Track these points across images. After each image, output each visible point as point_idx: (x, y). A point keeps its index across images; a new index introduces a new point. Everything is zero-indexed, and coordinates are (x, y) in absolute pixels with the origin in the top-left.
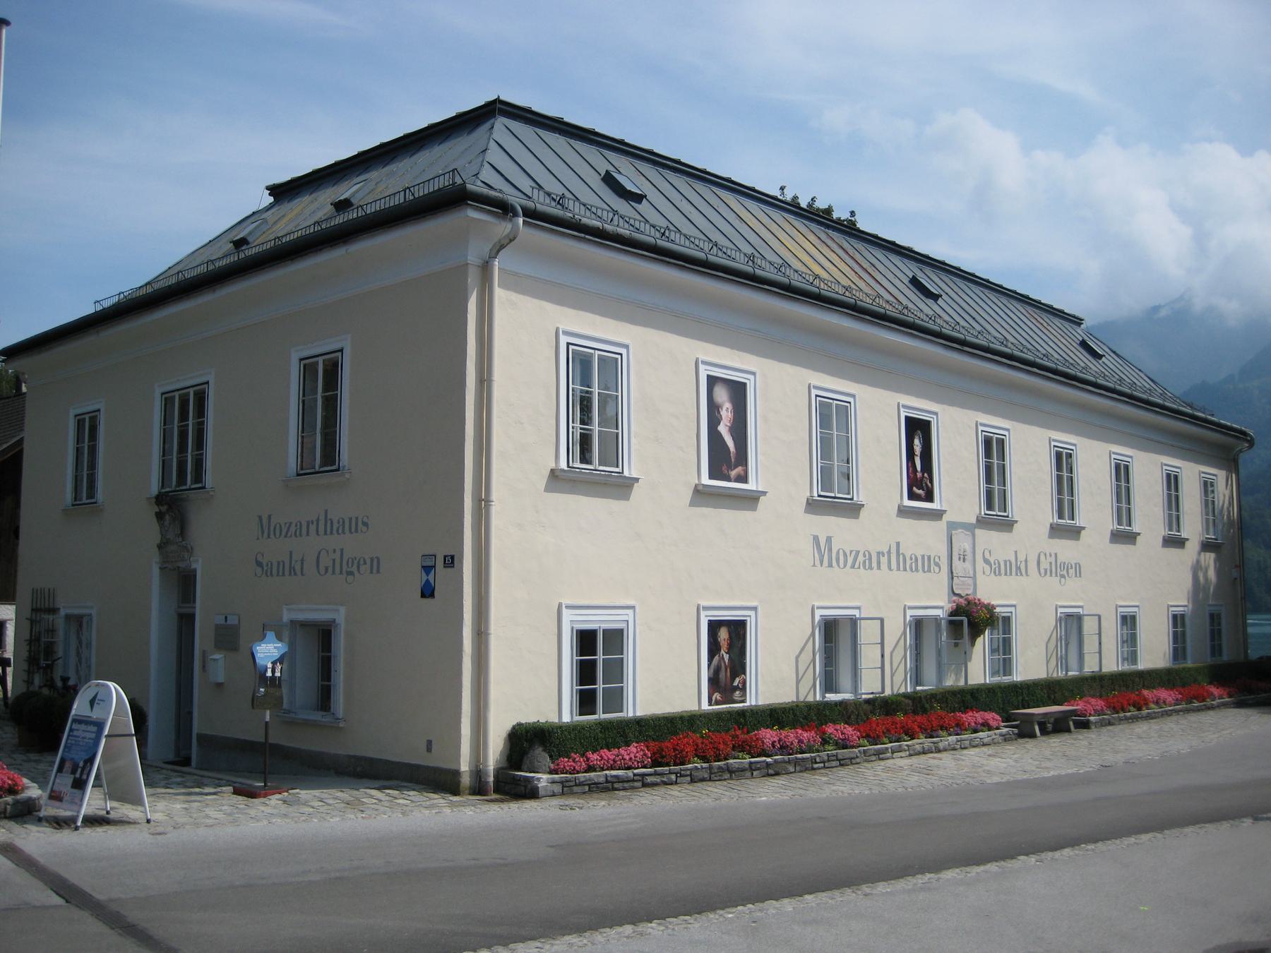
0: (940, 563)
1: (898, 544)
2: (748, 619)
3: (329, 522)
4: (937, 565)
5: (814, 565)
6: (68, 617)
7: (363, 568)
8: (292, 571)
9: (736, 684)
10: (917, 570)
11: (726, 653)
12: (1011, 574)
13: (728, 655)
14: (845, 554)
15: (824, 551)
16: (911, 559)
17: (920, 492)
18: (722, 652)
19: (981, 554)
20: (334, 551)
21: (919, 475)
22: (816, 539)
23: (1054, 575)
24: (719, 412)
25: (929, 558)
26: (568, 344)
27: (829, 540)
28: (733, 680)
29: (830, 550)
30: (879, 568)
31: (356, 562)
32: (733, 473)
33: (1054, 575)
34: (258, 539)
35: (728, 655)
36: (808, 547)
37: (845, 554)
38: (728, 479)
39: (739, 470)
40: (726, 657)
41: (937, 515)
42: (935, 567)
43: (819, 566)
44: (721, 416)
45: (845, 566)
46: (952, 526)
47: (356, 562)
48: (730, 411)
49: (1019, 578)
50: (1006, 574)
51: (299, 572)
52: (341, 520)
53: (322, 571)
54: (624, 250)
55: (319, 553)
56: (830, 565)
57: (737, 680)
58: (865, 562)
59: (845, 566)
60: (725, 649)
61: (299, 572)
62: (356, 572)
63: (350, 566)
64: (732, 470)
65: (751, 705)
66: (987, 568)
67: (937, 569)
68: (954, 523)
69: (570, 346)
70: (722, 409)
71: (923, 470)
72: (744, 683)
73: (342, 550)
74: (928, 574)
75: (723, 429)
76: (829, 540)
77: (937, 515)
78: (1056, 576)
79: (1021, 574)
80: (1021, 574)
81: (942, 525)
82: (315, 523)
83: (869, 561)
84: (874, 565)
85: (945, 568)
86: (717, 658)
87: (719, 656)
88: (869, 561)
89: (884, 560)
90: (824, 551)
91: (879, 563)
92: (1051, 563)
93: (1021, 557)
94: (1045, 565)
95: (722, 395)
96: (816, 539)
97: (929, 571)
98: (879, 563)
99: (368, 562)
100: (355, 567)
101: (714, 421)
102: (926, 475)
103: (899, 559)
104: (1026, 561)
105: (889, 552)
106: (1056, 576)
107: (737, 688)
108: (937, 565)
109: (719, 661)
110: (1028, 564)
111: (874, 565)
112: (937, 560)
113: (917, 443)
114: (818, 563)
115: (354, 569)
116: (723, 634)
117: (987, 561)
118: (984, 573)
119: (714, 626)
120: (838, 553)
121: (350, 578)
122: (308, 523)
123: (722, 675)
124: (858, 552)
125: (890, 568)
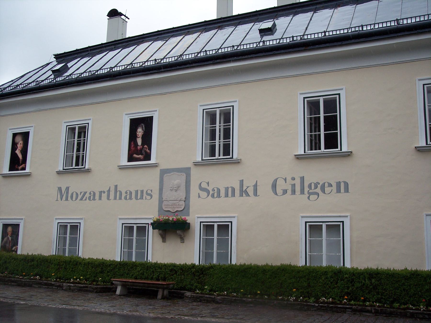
0: (152, 194)
2: (82, 222)
3: (118, 194)
5: (57, 200)
7: (327, 189)
8: (243, 192)
9: (13, 249)
11: (10, 237)
13: (11, 238)
14: (77, 194)
18: (9, 236)
22: (60, 189)
24: (17, 146)
26: (88, 123)
28: (12, 247)
29: (68, 193)
31: (319, 186)
32: (20, 167)
34: (57, 200)
35: (11, 238)
36: (55, 192)
38: (18, 170)
39: (23, 165)
40: (10, 238)
42: (147, 196)
43: (60, 200)
44: (17, 147)
45: (76, 199)
46: (163, 172)
48: (21, 144)
49: (245, 198)
52: (92, 193)
53: (279, 190)
54: (41, 91)
55: (276, 180)
56: (67, 199)
57: (14, 248)
58: (90, 197)
59: (76, 199)
60: (10, 235)
64: (20, 166)
65: (248, 265)
66: (204, 194)
69: (87, 124)
70: (18, 144)
71: (143, 144)
77: (155, 166)
78: (302, 192)
79: (248, 195)
80: (248, 195)
81: (156, 172)
82: (106, 193)
85: (156, 196)
87: (7, 238)
89: (104, 196)
95: (20, 141)
96: (60, 189)
99: (334, 185)
104: (255, 186)
105: (109, 191)
106: (302, 192)
107: (14, 251)
109: (7, 240)
115: (318, 190)
116: (10, 229)
119: (5, 226)
120: (72, 194)
121: (313, 197)
122: (101, 192)
124: (85, 193)
125: (108, 198)
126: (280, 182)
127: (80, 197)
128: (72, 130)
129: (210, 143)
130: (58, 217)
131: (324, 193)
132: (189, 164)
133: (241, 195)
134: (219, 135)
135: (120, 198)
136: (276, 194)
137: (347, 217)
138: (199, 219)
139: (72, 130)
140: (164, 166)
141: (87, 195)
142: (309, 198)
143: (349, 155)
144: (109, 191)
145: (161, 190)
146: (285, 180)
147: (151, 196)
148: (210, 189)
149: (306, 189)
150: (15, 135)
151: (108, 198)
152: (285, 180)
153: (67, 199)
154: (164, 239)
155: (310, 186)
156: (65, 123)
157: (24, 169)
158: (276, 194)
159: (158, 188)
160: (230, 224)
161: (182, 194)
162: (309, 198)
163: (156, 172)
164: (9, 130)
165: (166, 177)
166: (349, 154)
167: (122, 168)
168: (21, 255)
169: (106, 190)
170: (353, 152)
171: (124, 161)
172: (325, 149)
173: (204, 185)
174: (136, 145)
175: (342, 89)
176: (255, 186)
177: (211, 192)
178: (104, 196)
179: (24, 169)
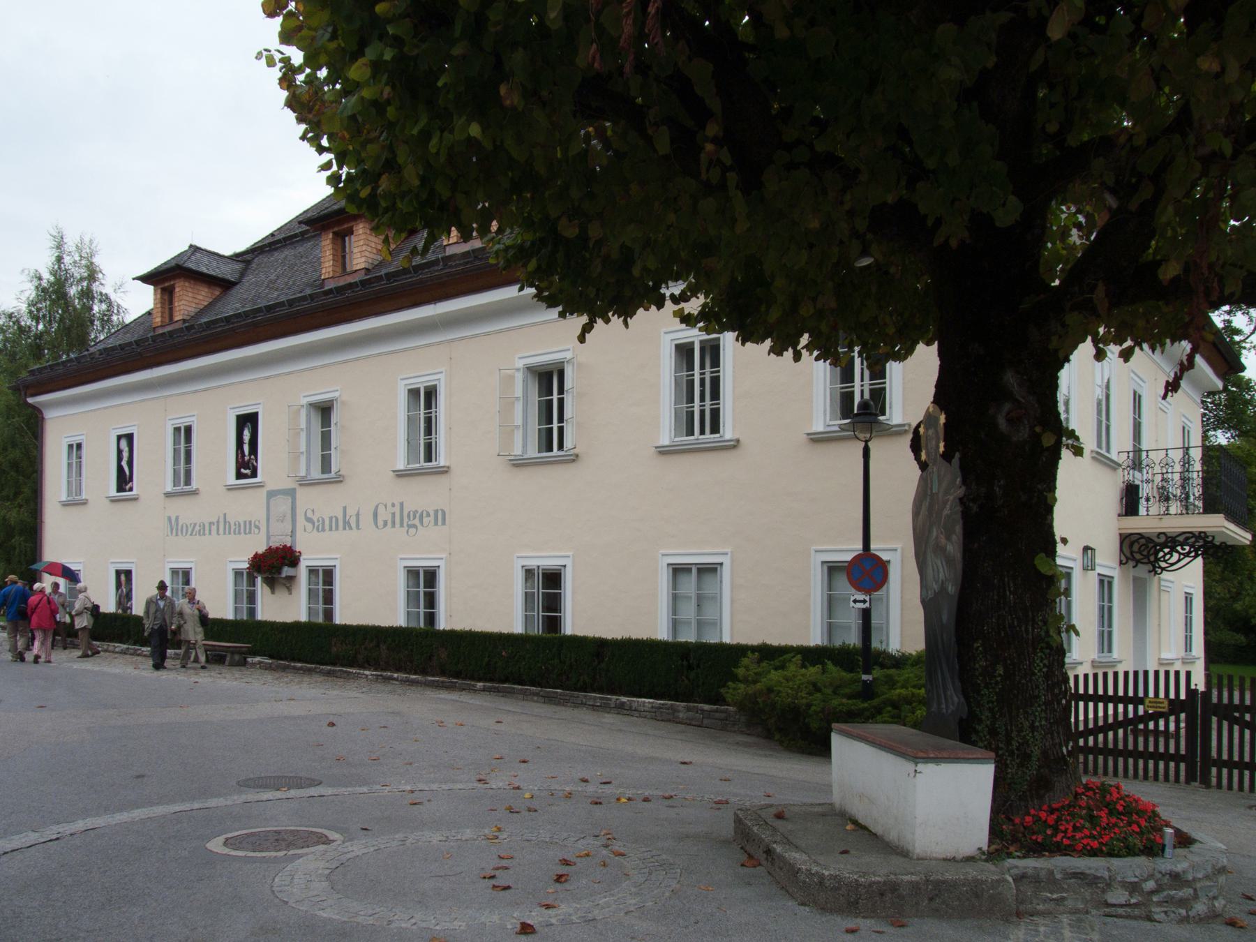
1: (225, 515)
4: (258, 528)
6: (313, 571)
7: (426, 520)
8: (347, 524)
10: (240, 533)
12: (337, 529)
14: (187, 526)
15: (174, 526)
16: (235, 525)
17: (247, 471)
19: (303, 514)
20: (393, 505)
21: (247, 458)
22: (169, 519)
23: (398, 525)
25: (250, 522)
27: (177, 518)
29: (177, 525)
30: (210, 534)
31: (418, 515)
33: (398, 525)
37: (187, 526)
40: (124, 590)
41: (260, 486)
45: (186, 534)
46: (271, 494)
47: (418, 515)
49: (348, 532)
50: (331, 529)
51: (354, 525)
53: (380, 523)
55: (377, 507)
56: (177, 535)
58: (200, 531)
59: (186, 534)
61: (354, 525)
62: (418, 525)
63: (412, 518)
66: (309, 526)
67: (257, 531)
68: (273, 491)
71: (250, 454)
72: (132, 605)
73: (402, 504)
74: (249, 536)
75: (124, 464)
76: (177, 518)
77: (260, 486)
78: (402, 525)
79: (351, 528)
80: (351, 528)
81: (262, 493)
83: (202, 530)
84: (207, 532)
85: (264, 529)
86: (120, 591)
88: (202, 530)
89: (214, 528)
90: (174, 526)
91: (210, 530)
92: (393, 514)
93: (351, 512)
94: (384, 515)
95: (124, 444)
96: (169, 519)
97: (250, 533)
98: (210, 530)
99: (432, 513)
100: (417, 519)
101: (120, 459)
102: (253, 457)
103: (225, 526)
104: (358, 515)
105: (218, 522)
106: (402, 525)
108: (258, 527)
110: (361, 518)
111: (207, 532)
112: (257, 523)
113: (247, 435)
114: (169, 533)
115: (417, 522)
117: (309, 520)
118: (305, 530)
121: (412, 531)
123: (122, 600)
124: (195, 525)
125: (218, 534)
126: (381, 510)
127: (190, 530)
128: (414, 393)
129: (687, 407)
130: (232, 559)
131: (422, 526)
132: (290, 484)
133: (345, 529)
134: (860, 371)
135: (230, 533)
136: (377, 527)
137: (727, 554)
138: (665, 558)
139: (414, 393)
140: (271, 486)
141: (197, 528)
142: (408, 532)
143: (574, 460)
144: (218, 522)
145: (268, 520)
146: (386, 506)
147: (259, 529)
148: (315, 519)
149: (406, 520)
150: (119, 438)
151: (218, 534)
152: (386, 506)
153: (177, 535)
154: (273, 591)
155: (409, 516)
156: (232, 411)
157: (131, 489)
158: (377, 527)
159: (265, 516)
160: (562, 568)
161: (288, 527)
162: (408, 532)
163: (262, 493)
164: (302, 398)
165: (272, 501)
166: (735, 445)
167: (231, 488)
168: (444, 631)
169: (215, 520)
170: (452, 467)
171: (232, 480)
172: (425, 462)
173: (310, 514)
174: (243, 455)
175: (442, 372)
176: (358, 515)
177: (316, 524)
178: (214, 528)
179: (131, 489)
